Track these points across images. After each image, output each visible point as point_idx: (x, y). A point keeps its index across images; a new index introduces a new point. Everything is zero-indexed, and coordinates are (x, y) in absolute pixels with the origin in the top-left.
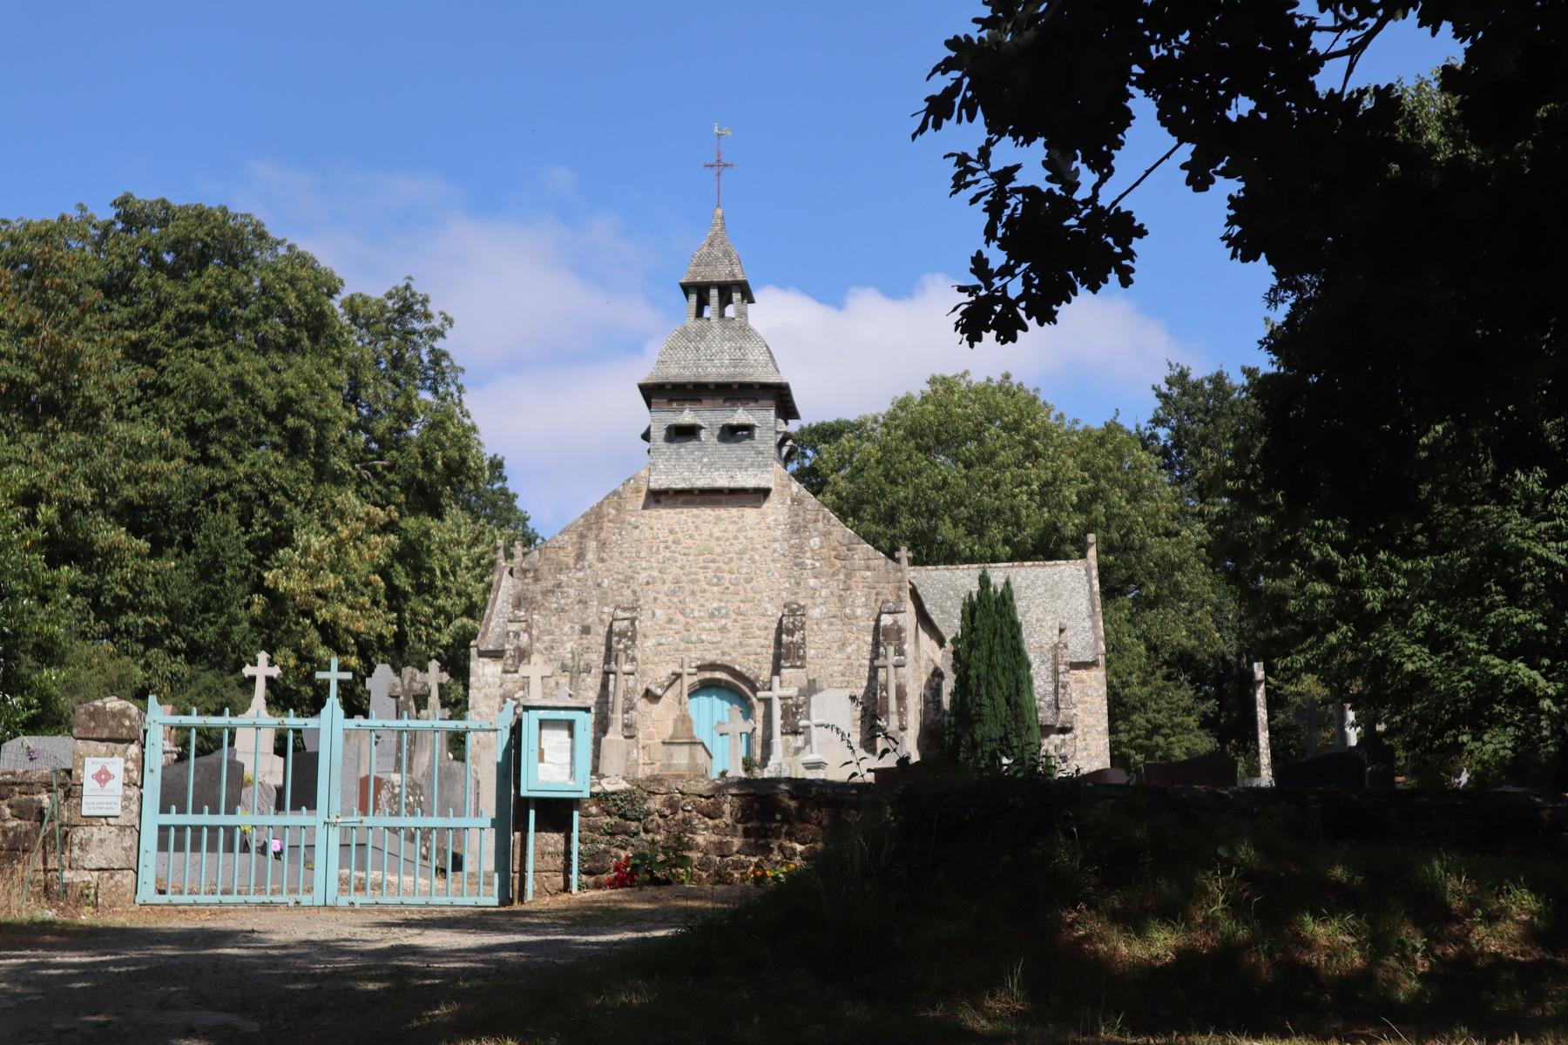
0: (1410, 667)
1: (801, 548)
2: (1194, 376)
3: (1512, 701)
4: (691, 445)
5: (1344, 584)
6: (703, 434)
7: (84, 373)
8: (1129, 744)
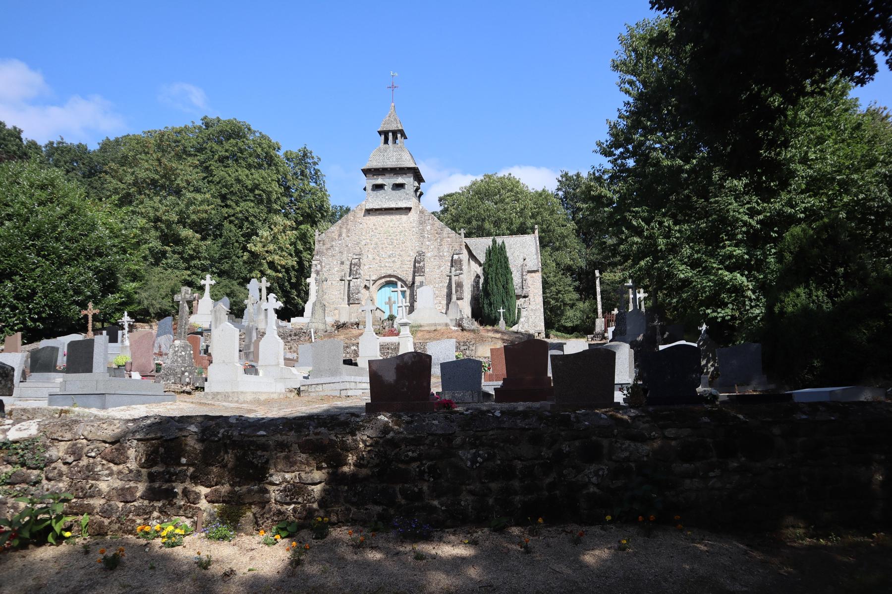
0: (682, 276)
1: (423, 230)
2: (570, 174)
3: (729, 291)
4: (381, 192)
5: (647, 238)
6: (386, 187)
7: (178, 175)
8: (550, 297)
